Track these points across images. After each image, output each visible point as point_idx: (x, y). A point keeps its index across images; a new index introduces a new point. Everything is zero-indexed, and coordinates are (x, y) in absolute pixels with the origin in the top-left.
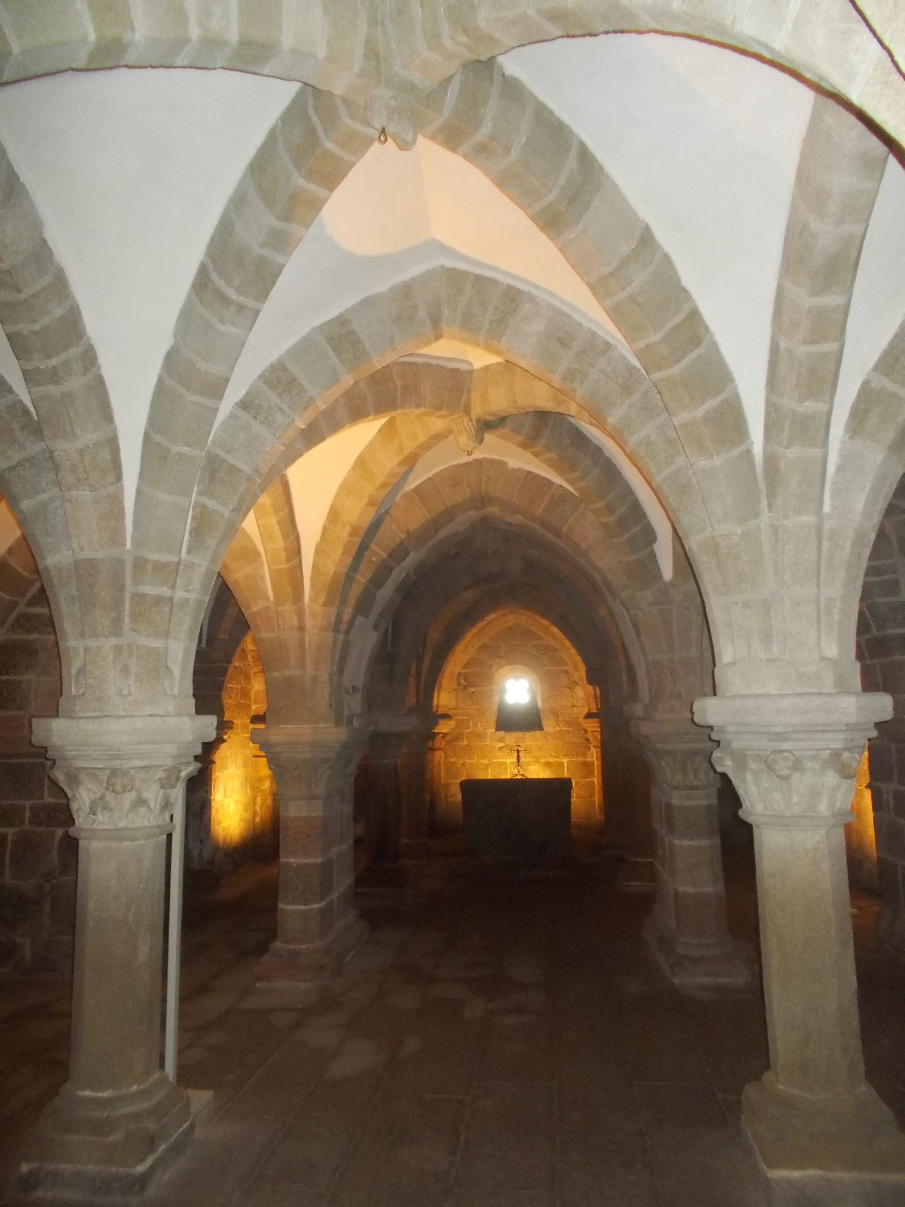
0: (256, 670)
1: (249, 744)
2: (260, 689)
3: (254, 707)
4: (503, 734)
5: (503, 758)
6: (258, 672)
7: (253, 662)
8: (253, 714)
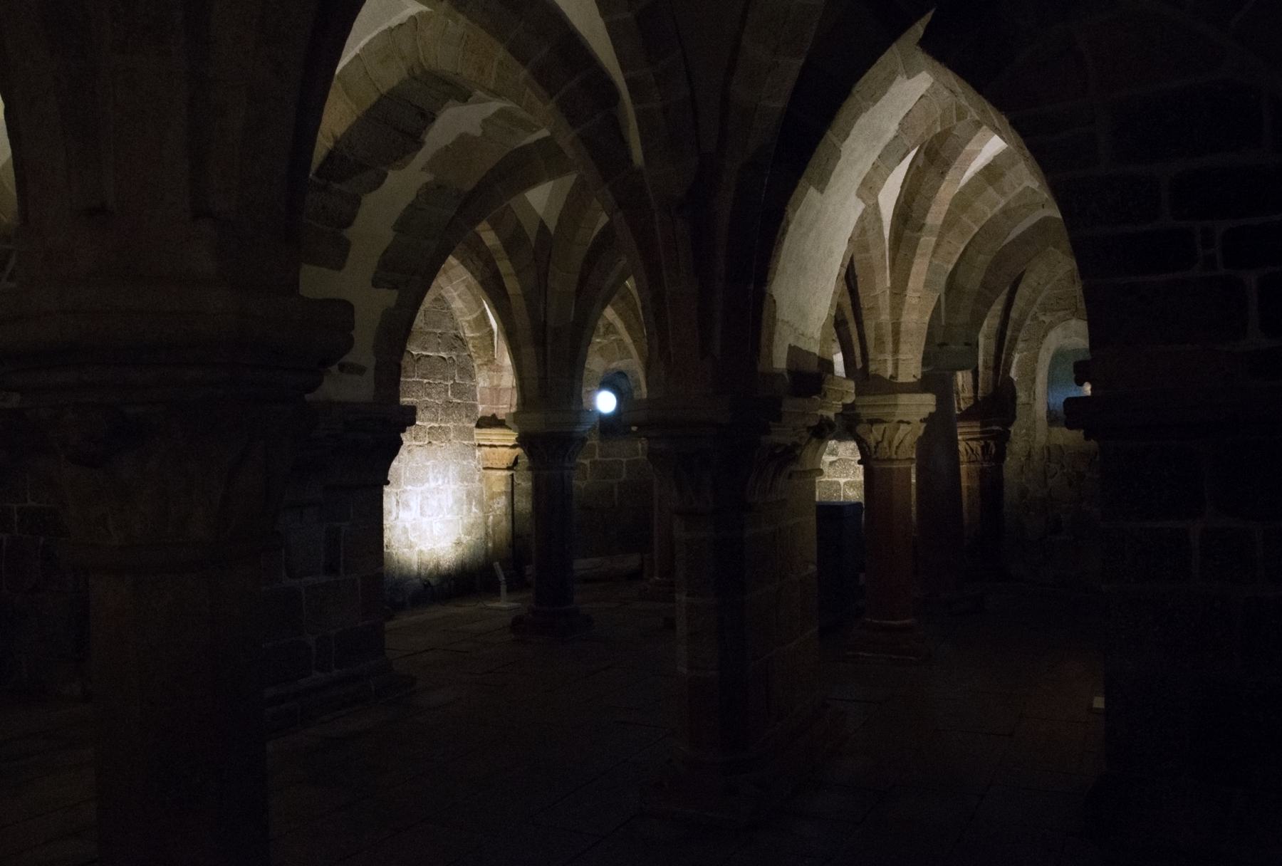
0: (479, 361)
1: (475, 453)
2: (486, 385)
3: (480, 408)
4: (835, 444)
5: (835, 477)
6: (482, 365)
7: (475, 353)
8: (479, 416)
